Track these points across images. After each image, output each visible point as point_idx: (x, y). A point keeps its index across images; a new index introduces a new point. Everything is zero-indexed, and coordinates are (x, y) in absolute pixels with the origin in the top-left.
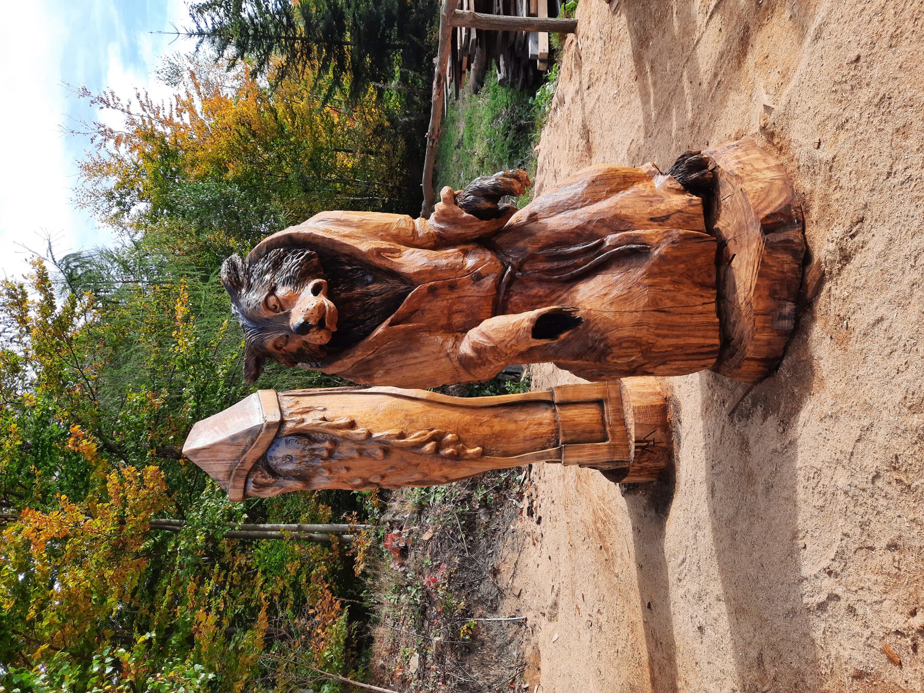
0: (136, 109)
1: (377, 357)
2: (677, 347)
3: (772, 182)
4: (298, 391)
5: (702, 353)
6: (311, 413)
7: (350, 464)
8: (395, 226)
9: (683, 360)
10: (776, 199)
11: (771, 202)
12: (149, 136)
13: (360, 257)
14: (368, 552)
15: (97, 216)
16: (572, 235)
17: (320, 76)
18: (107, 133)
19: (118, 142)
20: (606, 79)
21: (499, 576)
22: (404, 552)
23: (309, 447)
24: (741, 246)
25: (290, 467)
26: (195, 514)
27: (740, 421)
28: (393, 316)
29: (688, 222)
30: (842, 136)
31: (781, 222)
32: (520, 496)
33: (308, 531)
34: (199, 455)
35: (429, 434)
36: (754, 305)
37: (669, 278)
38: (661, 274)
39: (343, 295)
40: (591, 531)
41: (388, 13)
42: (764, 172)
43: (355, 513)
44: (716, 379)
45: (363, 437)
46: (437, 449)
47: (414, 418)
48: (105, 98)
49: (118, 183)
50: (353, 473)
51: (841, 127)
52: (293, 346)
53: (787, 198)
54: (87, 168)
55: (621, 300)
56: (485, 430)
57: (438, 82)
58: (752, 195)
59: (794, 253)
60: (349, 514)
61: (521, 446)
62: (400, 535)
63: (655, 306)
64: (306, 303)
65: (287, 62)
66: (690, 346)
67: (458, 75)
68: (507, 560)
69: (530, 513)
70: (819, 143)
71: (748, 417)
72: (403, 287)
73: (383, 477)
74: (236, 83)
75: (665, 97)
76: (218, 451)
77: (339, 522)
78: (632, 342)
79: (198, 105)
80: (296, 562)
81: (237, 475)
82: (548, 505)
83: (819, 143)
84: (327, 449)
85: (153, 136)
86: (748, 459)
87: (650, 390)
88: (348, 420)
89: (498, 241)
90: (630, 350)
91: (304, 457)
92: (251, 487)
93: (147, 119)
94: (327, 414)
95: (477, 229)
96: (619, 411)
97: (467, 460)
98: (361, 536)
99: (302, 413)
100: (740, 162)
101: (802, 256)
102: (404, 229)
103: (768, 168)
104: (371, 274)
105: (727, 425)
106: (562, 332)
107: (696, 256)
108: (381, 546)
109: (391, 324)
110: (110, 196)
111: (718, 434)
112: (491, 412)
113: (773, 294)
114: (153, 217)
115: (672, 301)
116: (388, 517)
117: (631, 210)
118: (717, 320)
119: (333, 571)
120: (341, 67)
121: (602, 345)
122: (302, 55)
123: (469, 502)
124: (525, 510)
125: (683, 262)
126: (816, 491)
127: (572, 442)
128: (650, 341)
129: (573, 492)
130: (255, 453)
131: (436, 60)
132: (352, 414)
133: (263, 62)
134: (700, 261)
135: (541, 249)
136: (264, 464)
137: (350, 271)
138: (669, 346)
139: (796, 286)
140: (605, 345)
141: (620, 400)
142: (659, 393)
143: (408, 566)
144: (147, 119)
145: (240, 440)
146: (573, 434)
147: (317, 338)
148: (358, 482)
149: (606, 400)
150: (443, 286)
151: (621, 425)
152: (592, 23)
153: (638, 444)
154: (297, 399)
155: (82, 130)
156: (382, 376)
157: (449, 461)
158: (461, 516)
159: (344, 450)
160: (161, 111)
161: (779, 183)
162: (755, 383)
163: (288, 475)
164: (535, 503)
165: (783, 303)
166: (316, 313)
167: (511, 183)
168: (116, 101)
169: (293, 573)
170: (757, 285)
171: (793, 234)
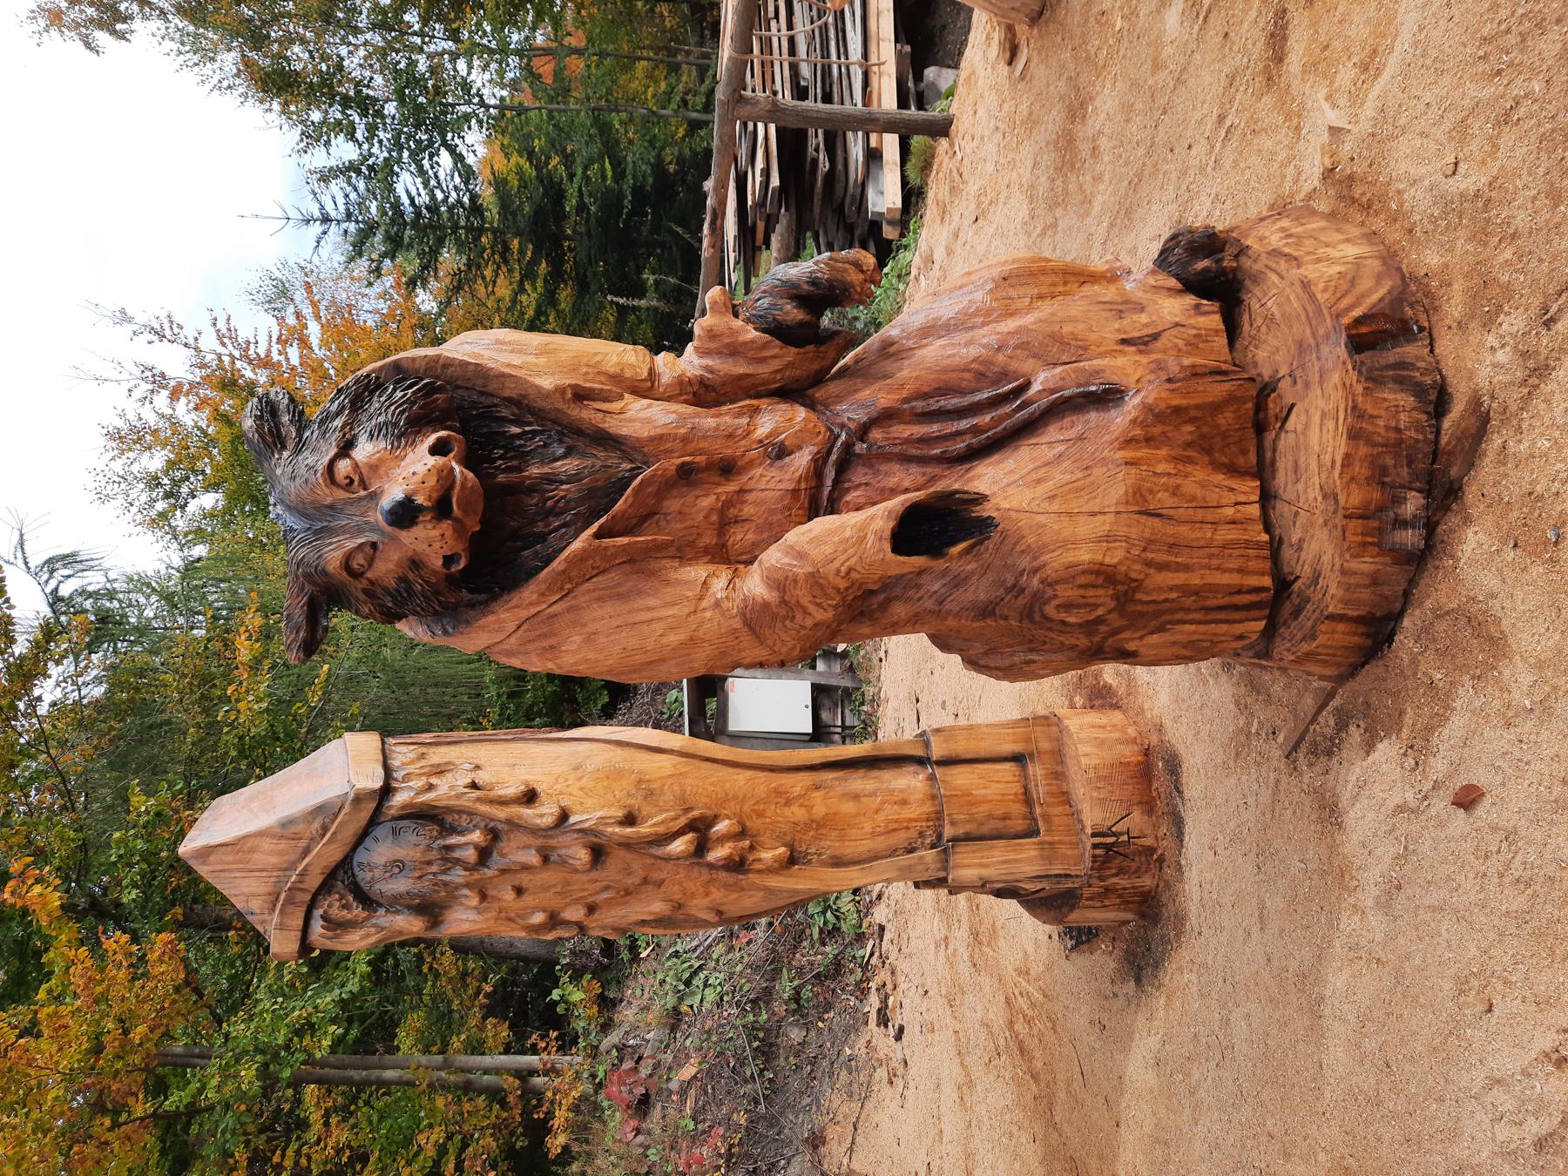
0: (209, 343)
1: (570, 609)
2: (1186, 590)
3: (1358, 262)
4: (426, 737)
5: (1236, 608)
6: (449, 775)
7: (524, 879)
8: (615, 359)
9: (1199, 623)
10: (1371, 291)
11: (1363, 296)
12: (229, 383)
13: (540, 404)
14: (575, 1108)
15: (129, 517)
16: (967, 375)
17: (522, 290)
18: (159, 380)
19: (175, 394)
20: (1008, 198)
21: (822, 1150)
22: (643, 1105)
23: (441, 842)
24: (1307, 385)
25: (400, 885)
26: (243, 1026)
27: (1311, 765)
28: (602, 520)
29: (1195, 346)
30: (1508, 138)
31: (1384, 331)
32: (862, 991)
33: (463, 1070)
34: (212, 858)
35: (683, 821)
36: (1342, 499)
37: (1164, 452)
38: (1148, 440)
39: (501, 478)
40: (1002, 1042)
41: (638, 191)
42: (1341, 247)
43: (553, 1034)
44: (1254, 687)
45: (548, 821)
46: (701, 848)
47: (654, 786)
48: (157, 326)
49: (169, 461)
50: (528, 900)
51: (1505, 119)
52: (386, 568)
53: (1393, 288)
54: (117, 436)
55: (1069, 491)
56: (797, 813)
57: (713, 222)
58: (1321, 285)
59: (1419, 391)
60: (542, 1037)
61: (865, 846)
62: (635, 1070)
63: (1141, 504)
64: (415, 468)
65: (469, 265)
66: (1213, 589)
67: (750, 253)
68: (840, 1118)
69: (883, 1021)
70: (1456, 164)
71: (1329, 754)
72: (626, 466)
73: (591, 909)
74: (383, 306)
75: (1122, 191)
76: (252, 850)
77: (523, 1052)
78: (1098, 573)
79: (314, 330)
80: (437, 1129)
81: (290, 901)
82: (918, 1000)
83: (1456, 164)
84: (476, 847)
85: (234, 383)
86: (1338, 838)
87: (1116, 735)
88: (522, 788)
89: (819, 394)
90: (1091, 592)
91: (429, 863)
92: (317, 927)
93: (226, 359)
94: (482, 777)
95: (776, 365)
96: (1058, 776)
97: (759, 871)
98: (563, 1076)
99: (429, 775)
100: (1290, 236)
101: (1433, 397)
102: (631, 366)
103: (1347, 240)
104: (561, 442)
105: (1284, 779)
106: (954, 543)
107: (1216, 408)
108: (601, 1096)
109: (598, 535)
110: (153, 481)
111: (1265, 797)
112: (806, 779)
113: (1379, 476)
114: (223, 517)
115: (1174, 494)
116: (614, 1037)
117: (1081, 326)
118: (1266, 537)
119: (509, 1153)
120: (556, 276)
121: (1035, 581)
122: (493, 254)
123: (767, 1003)
124: (873, 1017)
125: (1192, 420)
126: (1507, 880)
127: (968, 838)
128: (1133, 575)
129: (964, 968)
130: (326, 854)
131: (708, 185)
132: (529, 777)
133: (429, 264)
134: (1226, 419)
135: (906, 400)
136: (342, 877)
137: (518, 436)
138: (1171, 589)
139: (1425, 471)
140: (1042, 581)
141: (1058, 755)
142: (1134, 741)
143: (649, 1133)
144: (226, 359)
145: (300, 828)
146: (968, 822)
147: (430, 542)
148: (538, 918)
149: (1031, 755)
150: (709, 467)
151: (1062, 803)
152: (980, 112)
153: (1098, 840)
154: (424, 750)
155: (115, 375)
156: (579, 649)
157: (723, 875)
158: (751, 1029)
159: (517, 852)
160: (252, 346)
161: (1374, 265)
162: (1341, 680)
163: (395, 903)
164: (891, 1001)
165: (1401, 492)
166: (432, 481)
167: (845, 270)
168: (176, 330)
169: (430, 1152)
170: (1347, 456)
171: (1412, 351)
